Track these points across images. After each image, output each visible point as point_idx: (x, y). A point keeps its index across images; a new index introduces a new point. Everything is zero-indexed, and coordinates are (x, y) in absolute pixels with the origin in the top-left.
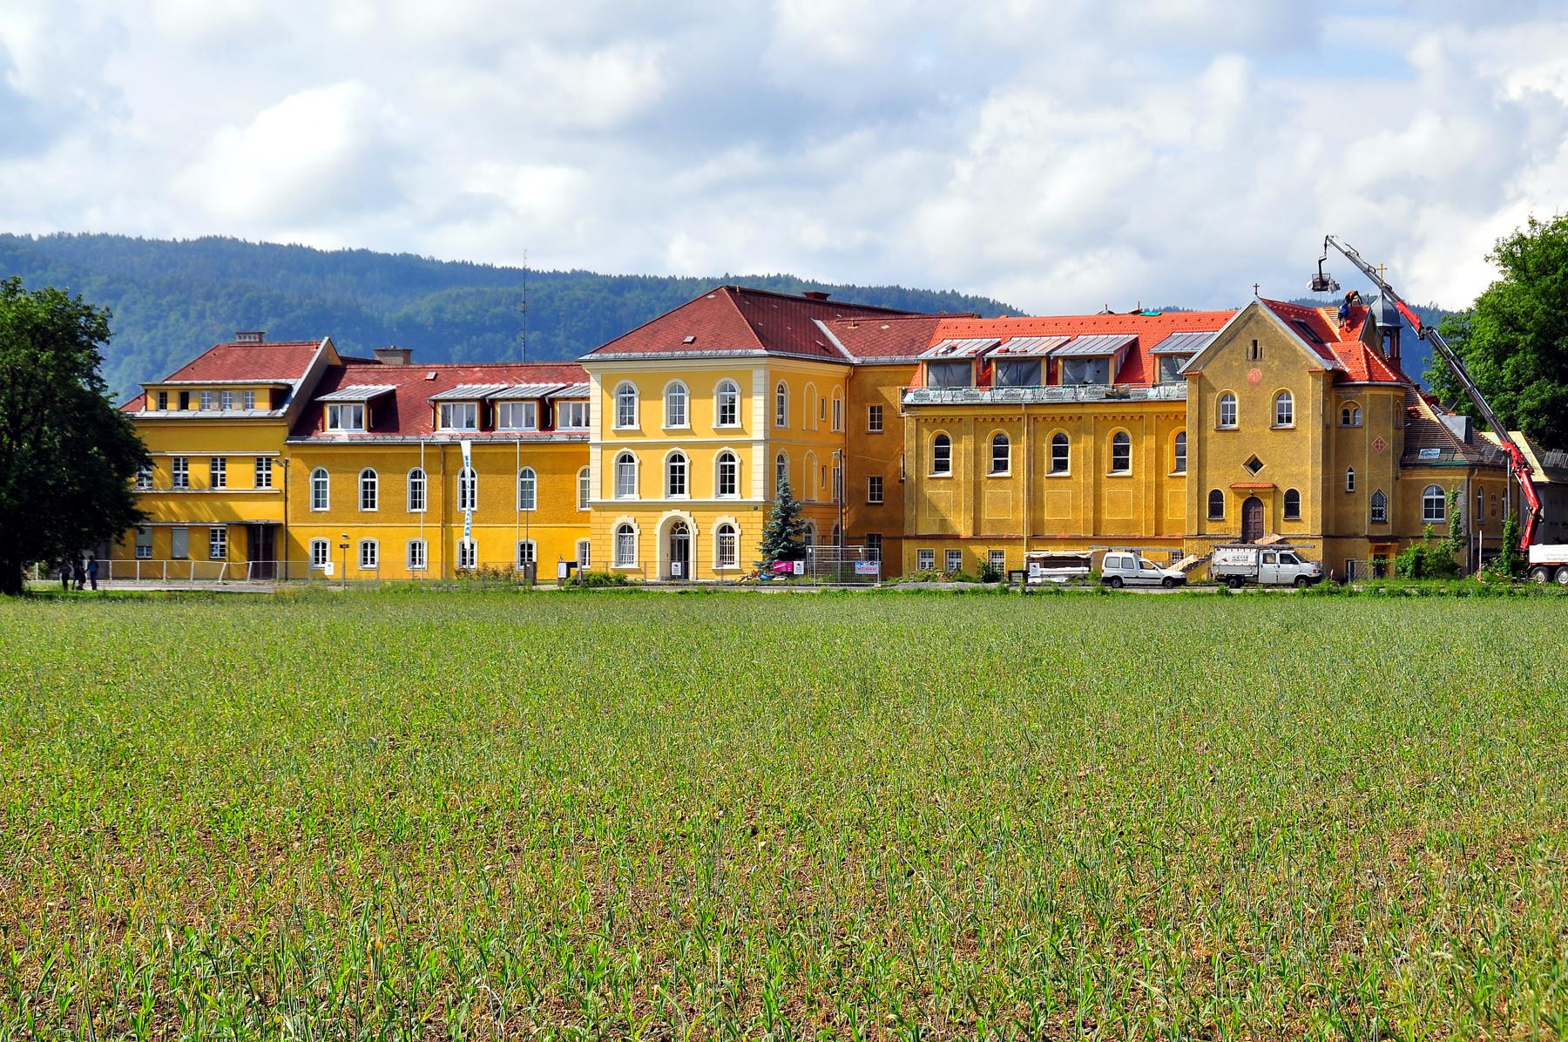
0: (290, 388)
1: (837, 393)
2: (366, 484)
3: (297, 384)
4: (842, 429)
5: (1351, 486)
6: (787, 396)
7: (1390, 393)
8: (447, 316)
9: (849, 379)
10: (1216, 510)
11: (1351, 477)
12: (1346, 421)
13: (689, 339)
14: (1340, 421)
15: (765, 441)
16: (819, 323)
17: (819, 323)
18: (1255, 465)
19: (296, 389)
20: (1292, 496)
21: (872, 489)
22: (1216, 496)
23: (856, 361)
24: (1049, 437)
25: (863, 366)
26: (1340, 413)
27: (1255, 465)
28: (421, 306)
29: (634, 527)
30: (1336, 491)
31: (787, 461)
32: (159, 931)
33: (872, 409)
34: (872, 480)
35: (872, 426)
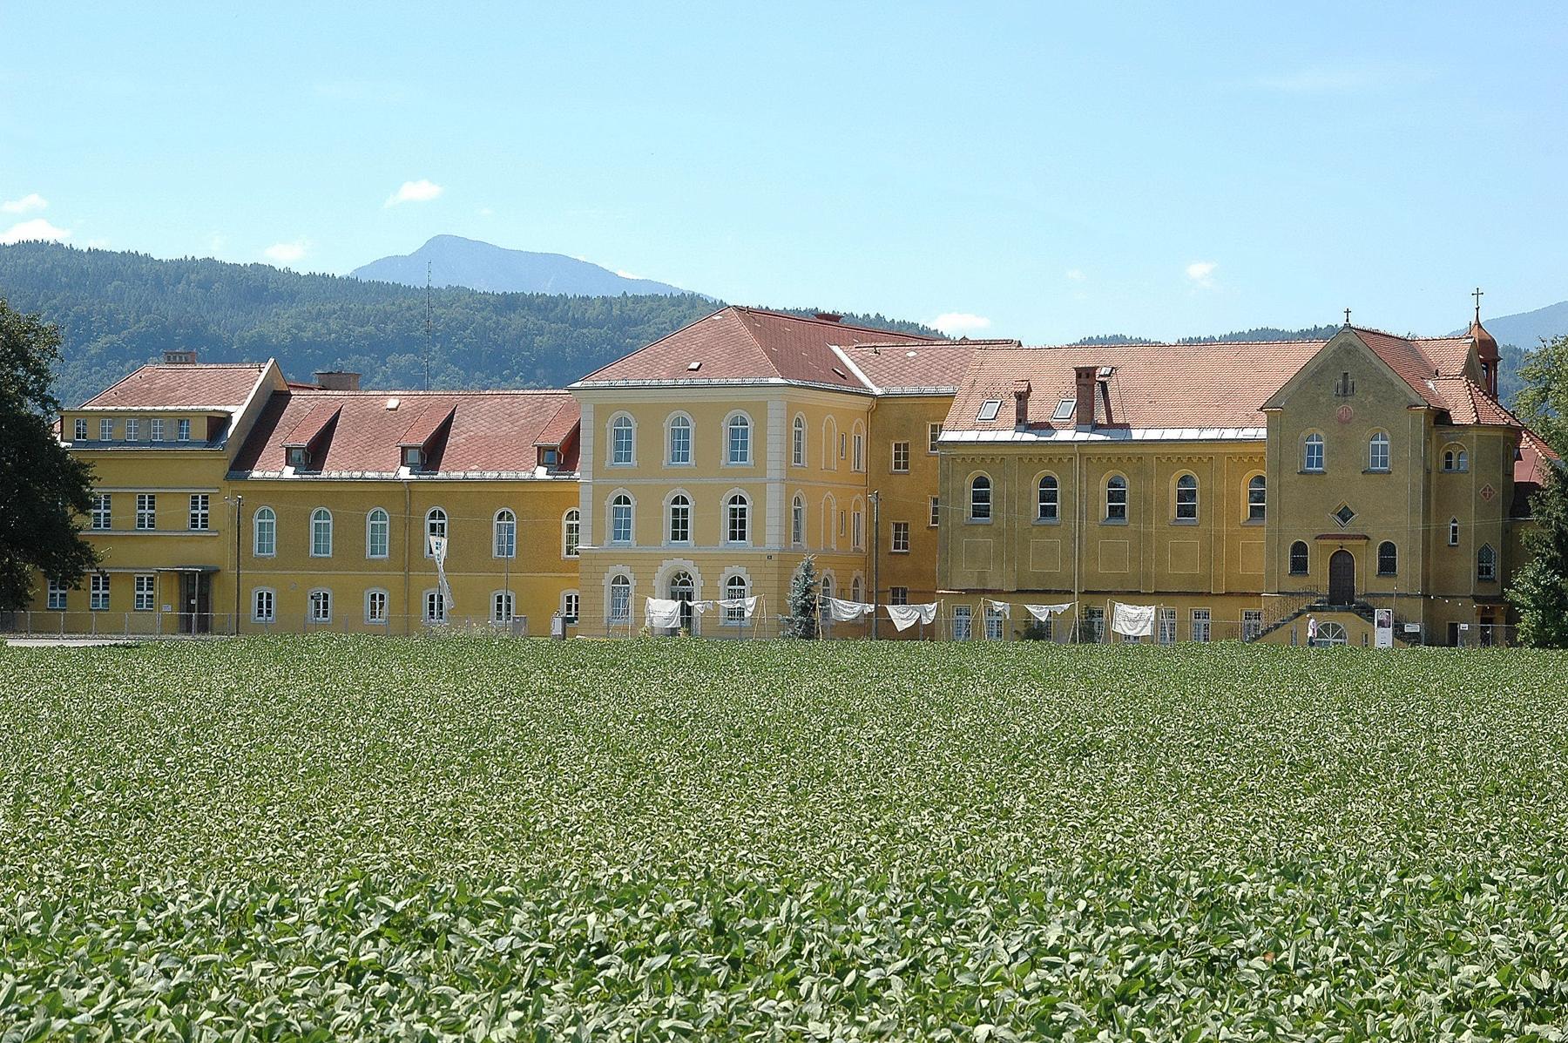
0: (229, 415)
1: (859, 430)
2: (676, 512)
3: (238, 412)
4: (863, 468)
5: (1455, 539)
6: (804, 430)
7: (1500, 434)
8: (307, 335)
9: (871, 412)
10: (1299, 566)
11: (1455, 529)
12: (1449, 465)
13: (695, 365)
14: (1442, 465)
15: (782, 481)
16: (836, 349)
17: (836, 349)
18: (1345, 515)
19: (236, 420)
20: (1388, 550)
21: (897, 537)
22: (1299, 548)
23: (878, 391)
24: (969, 481)
25: (886, 397)
26: (1442, 456)
27: (1345, 515)
28: (1294, 387)
29: (630, 577)
30: (1435, 546)
31: (804, 505)
32: (777, 881)
33: (897, 447)
34: (898, 526)
35: (897, 466)
